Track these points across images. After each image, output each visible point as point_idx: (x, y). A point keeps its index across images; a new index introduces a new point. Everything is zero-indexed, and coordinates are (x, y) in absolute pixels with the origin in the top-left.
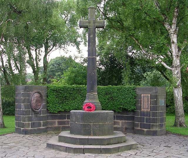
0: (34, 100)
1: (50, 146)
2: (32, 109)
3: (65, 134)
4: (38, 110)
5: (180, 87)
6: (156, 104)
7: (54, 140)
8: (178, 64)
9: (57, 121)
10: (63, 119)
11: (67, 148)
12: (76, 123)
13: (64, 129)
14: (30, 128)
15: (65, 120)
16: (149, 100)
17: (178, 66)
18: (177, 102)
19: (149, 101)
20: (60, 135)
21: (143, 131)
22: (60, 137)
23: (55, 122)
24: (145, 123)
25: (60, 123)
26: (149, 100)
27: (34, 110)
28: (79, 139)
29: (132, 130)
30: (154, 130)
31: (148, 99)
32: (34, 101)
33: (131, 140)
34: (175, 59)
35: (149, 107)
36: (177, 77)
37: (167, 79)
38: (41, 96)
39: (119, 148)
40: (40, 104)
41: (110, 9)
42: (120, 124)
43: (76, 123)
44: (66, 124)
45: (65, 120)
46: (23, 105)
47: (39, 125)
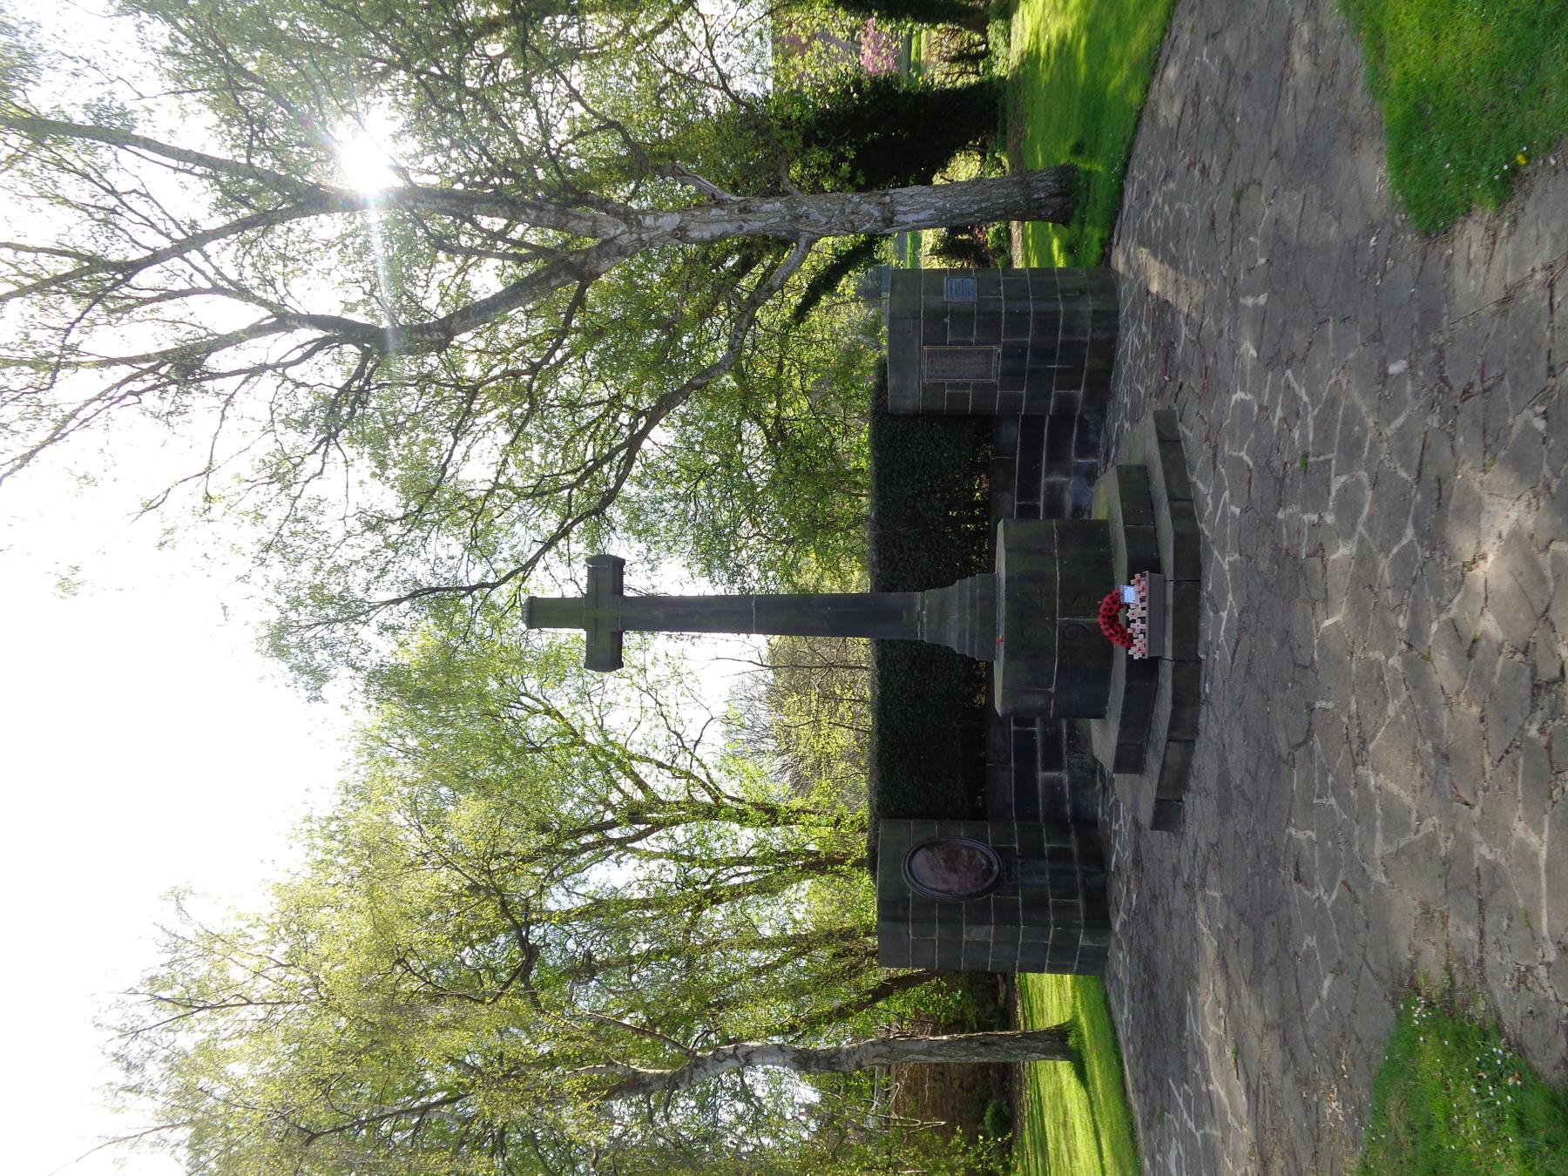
0: (946, 881)
1: (1167, 815)
3: (1104, 739)
5: (888, 199)
6: (969, 315)
7: (1132, 798)
9: (1042, 775)
12: (1053, 689)
14: (1081, 903)
15: (1039, 738)
16: (947, 348)
17: (790, 208)
22: (1120, 766)
23: (1051, 785)
25: (1053, 762)
26: (947, 348)
27: (991, 881)
28: (1128, 680)
29: (1075, 429)
30: (1089, 323)
33: (1137, 440)
34: (755, 225)
37: (88, 136)
38: (929, 845)
39: (1172, 498)
40: (964, 851)
41: (843, 836)
42: (1058, 478)
43: (1053, 689)
45: (1039, 738)
46: (968, 933)
47: (1060, 855)
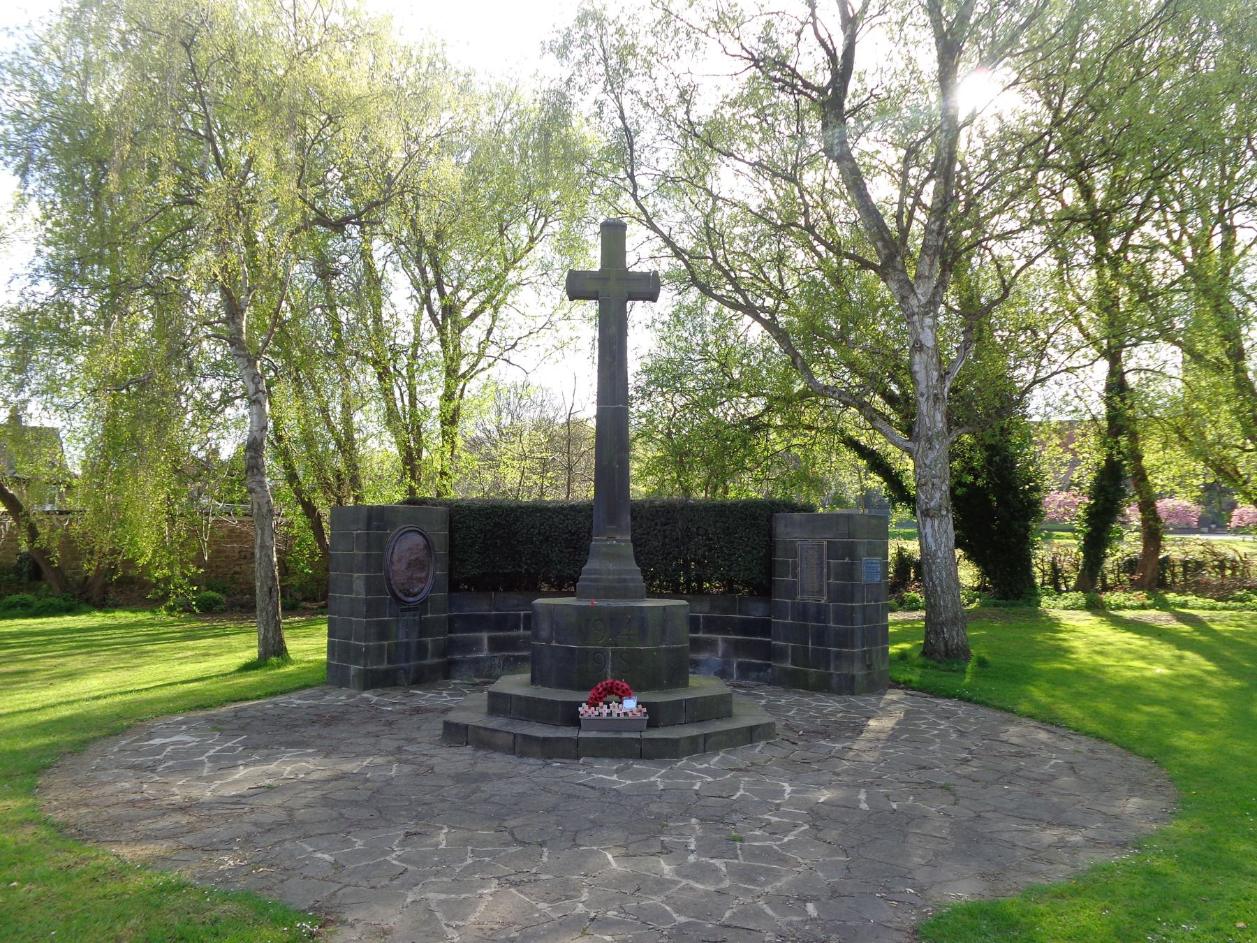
0: (399, 560)
1: (456, 734)
2: (394, 594)
3: (515, 684)
4: (415, 595)
5: (944, 513)
6: (852, 578)
7: (469, 706)
8: (940, 425)
9: (485, 636)
10: (511, 629)
11: (519, 740)
13: (512, 665)
15: (514, 633)
18: (931, 571)
19: (825, 565)
20: (492, 688)
21: (805, 674)
22: (493, 696)
23: (477, 643)
24: (720, 637)
25: (496, 645)
31: (821, 557)
32: (403, 566)
33: (751, 709)
34: (924, 407)
35: (825, 588)
36: (934, 477)
38: (429, 546)
43: (554, 644)
44: (519, 649)
